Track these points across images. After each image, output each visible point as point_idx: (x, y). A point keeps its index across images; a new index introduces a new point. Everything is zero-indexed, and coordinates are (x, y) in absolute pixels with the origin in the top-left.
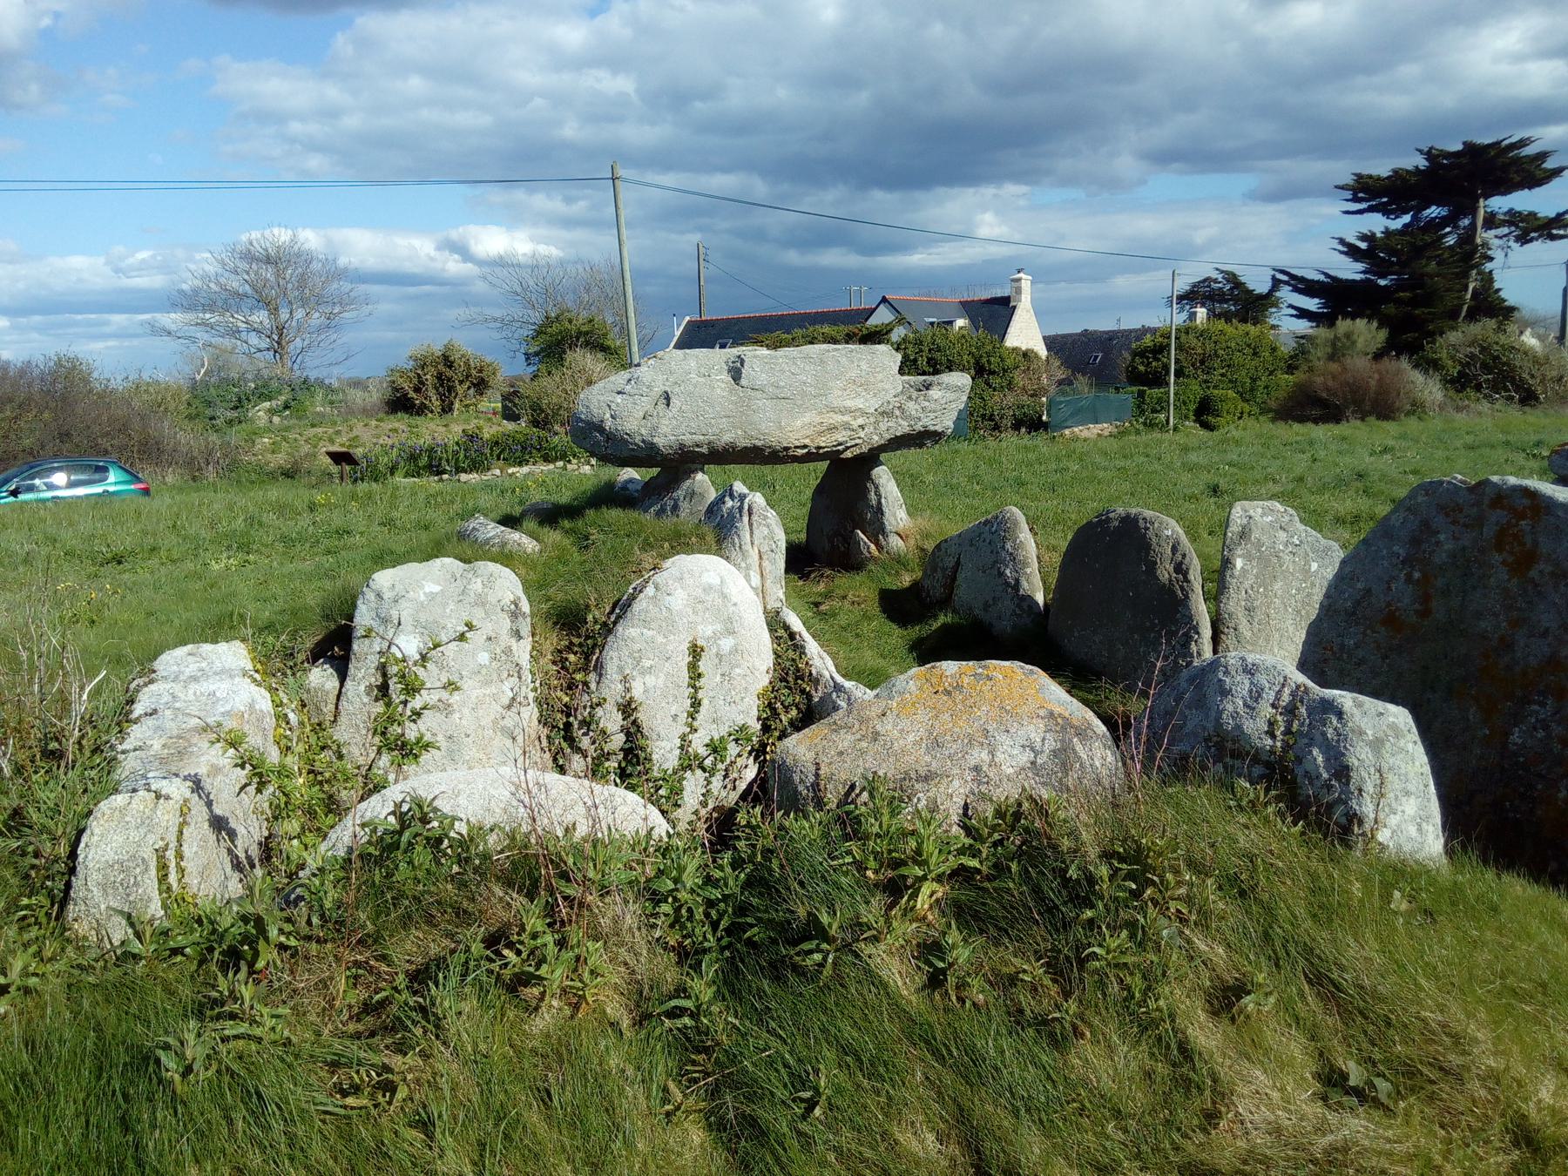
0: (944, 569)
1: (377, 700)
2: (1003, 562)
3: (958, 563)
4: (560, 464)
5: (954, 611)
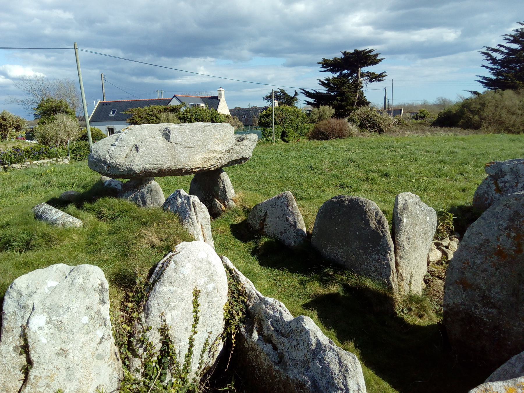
0: (259, 217)
1: (21, 354)
2: (288, 215)
3: (266, 214)
4: (55, 159)
5: (267, 236)
